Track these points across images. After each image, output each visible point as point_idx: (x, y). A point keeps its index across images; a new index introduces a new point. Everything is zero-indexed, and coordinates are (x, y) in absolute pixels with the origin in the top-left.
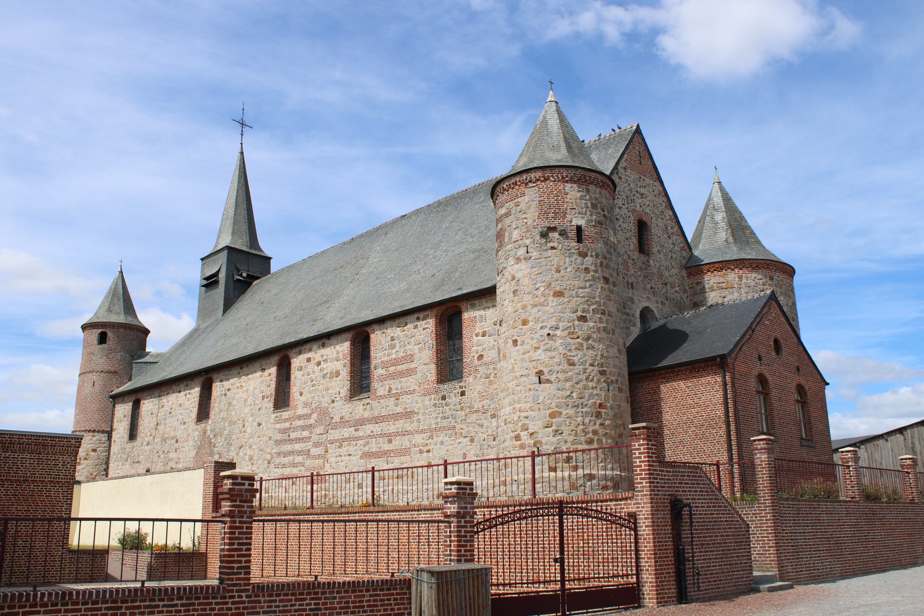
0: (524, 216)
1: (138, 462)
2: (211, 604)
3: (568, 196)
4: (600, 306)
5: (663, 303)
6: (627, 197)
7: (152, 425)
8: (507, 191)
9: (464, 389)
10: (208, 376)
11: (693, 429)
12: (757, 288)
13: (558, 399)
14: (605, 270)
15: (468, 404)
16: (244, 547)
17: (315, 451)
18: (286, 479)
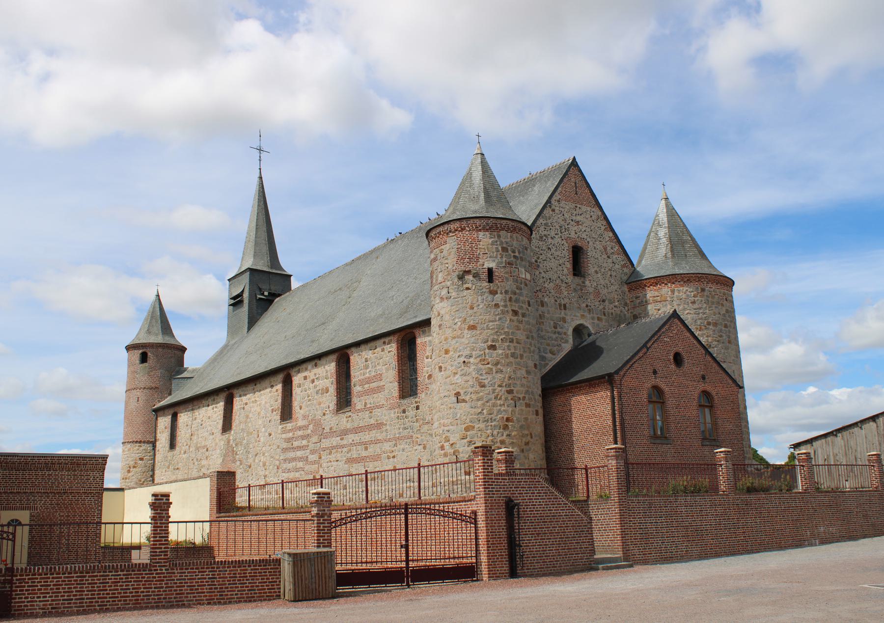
0: (446, 261)
1: (178, 468)
2: (142, 574)
3: (481, 243)
5: (599, 319)
6: (561, 227)
7: (188, 435)
10: (230, 391)
11: (591, 436)
12: (688, 300)
14: (514, 304)
16: (163, 539)
17: (312, 458)
18: (291, 482)
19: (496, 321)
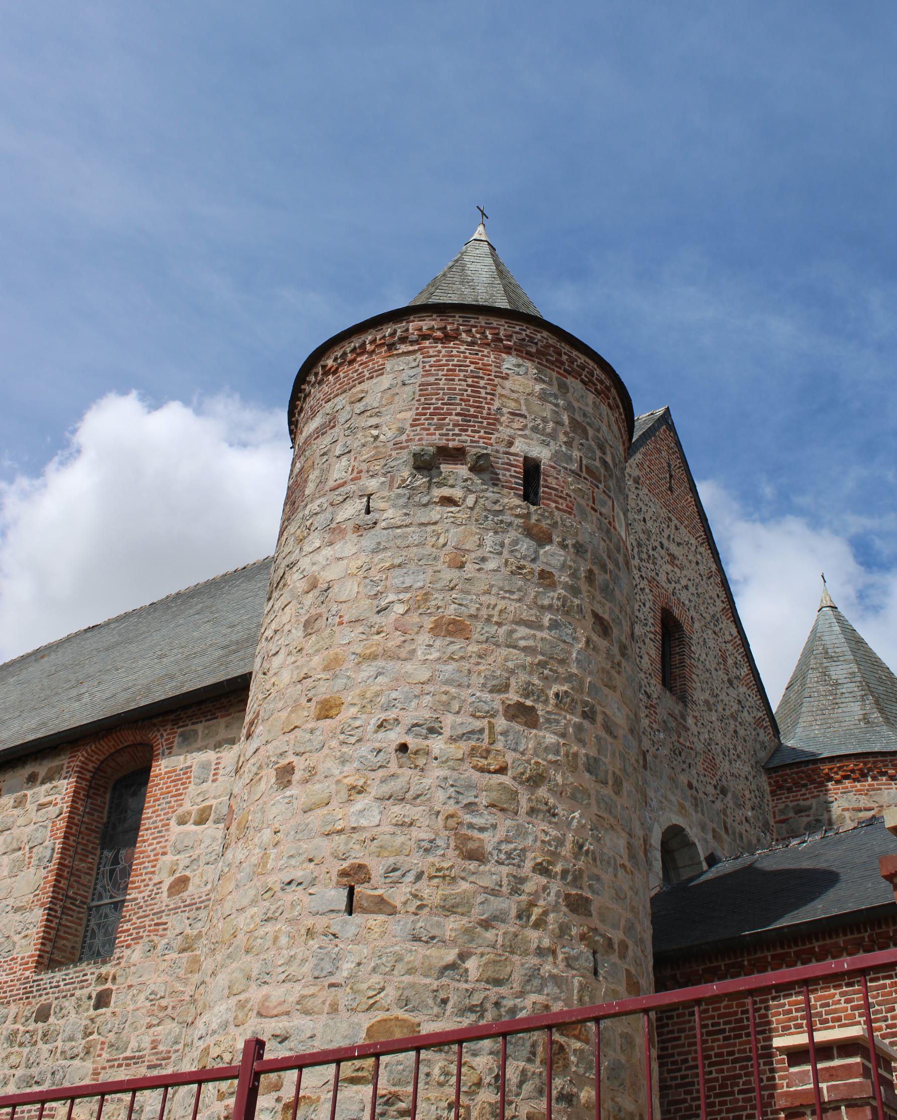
0: (374, 421)
4: (580, 690)
8: (335, 372)
9: (109, 985)
13: (410, 971)
15: (112, 1037)
19: (540, 627)
